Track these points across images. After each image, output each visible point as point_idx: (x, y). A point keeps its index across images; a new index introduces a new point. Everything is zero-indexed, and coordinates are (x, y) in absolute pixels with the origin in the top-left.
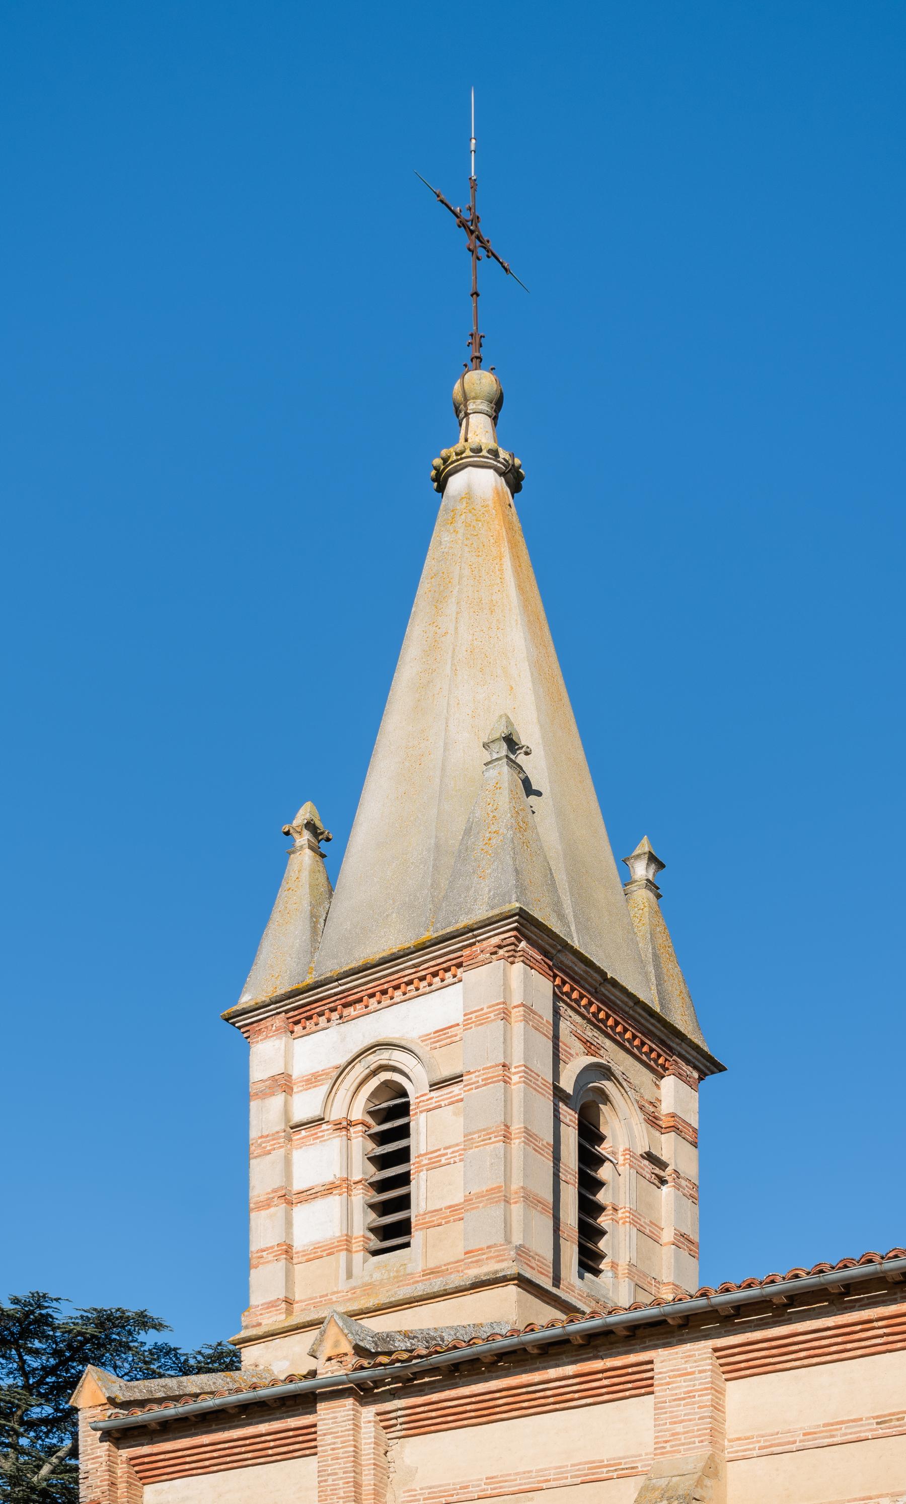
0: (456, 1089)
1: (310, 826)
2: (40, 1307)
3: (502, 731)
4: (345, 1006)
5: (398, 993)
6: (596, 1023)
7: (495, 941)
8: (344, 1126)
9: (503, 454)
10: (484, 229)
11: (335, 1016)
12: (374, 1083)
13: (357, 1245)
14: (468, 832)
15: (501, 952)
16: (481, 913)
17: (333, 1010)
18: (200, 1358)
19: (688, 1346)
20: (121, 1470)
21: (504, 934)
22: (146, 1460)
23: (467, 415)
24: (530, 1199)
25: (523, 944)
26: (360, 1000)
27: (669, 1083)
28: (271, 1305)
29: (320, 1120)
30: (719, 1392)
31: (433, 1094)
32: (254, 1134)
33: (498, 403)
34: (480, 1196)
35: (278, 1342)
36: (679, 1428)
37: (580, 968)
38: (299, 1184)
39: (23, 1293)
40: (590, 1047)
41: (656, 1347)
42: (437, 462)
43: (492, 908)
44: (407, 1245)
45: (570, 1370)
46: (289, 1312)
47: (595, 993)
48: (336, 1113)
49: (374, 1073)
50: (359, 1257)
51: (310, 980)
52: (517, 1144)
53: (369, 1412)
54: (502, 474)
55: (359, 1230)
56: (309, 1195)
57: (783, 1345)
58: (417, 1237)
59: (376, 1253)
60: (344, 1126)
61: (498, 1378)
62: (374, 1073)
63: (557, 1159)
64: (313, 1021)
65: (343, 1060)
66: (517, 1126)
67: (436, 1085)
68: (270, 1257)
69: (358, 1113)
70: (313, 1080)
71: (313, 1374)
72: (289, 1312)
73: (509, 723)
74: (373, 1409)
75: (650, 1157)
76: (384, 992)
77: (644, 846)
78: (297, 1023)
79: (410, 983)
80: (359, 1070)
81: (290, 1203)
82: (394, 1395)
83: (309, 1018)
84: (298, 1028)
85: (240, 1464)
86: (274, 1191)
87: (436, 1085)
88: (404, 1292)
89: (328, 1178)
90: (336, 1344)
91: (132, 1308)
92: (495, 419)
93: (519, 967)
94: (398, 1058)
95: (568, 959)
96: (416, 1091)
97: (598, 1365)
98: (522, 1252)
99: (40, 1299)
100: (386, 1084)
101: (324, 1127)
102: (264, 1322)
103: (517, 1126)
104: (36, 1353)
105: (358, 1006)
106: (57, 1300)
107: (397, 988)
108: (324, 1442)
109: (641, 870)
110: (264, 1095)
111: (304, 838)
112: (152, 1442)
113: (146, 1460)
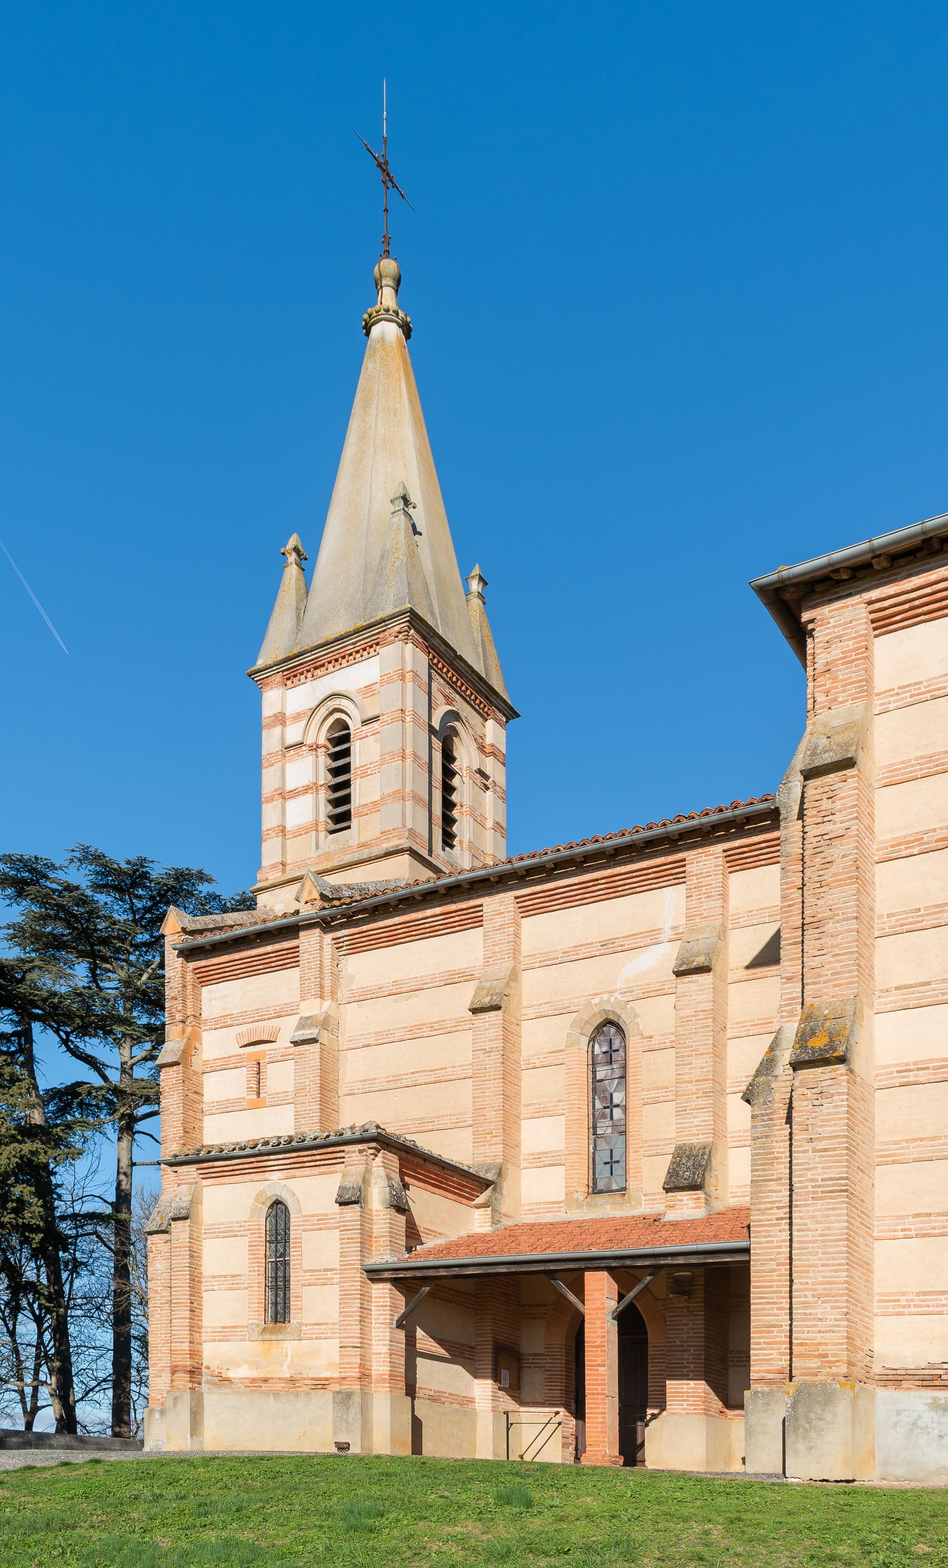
0: (376, 725)
1: (296, 550)
2: (143, 866)
3: (400, 493)
4: (316, 668)
5: (344, 661)
6: (451, 684)
7: (397, 628)
8: (315, 748)
9: (401, 314)
10: (391, 169)
11: (309, 675)
12: (331, 720)
13: (321, 828)
14: (382, 557)
15: (400, 636)
16: (390, 610)
17: (308, 671)
18: (233, 902)
19: (501, 895)
20: (189, 976)
21: (400, 625)
22: (203, 970)
23: (381, 287)
24: (416, 798)
25: (412, 631)
26: (323, 665)
27: (490, 723)
28: (274, 866)
29: (301, 744)
30: (518, 925)
31: (364, 728)
32: (264, 752)
33: (398, 281)
34: (389, 795)
35: (278, 891)
36: (497, 949)
37: (442, 648)
38: (289, 787)
39: (133, 858)
40: (449, 701)
41: (484, 896)
42: (366, 316)
43: (396, 607)
44: (349, 827)
45: (438, 910)
46: (284, 871)
47: (451, 665)
48: (310, 740)
49: (331, 713)
50: (322, 834)
51: (295, 651)
52: (409, 761)
53: (328, 938)
54: (400, 326)
55: (323, 818)
56: (295, 793)
57: (551, 895)
58: (354, 822)
59: (332, 832)
60: (315, 748)
61: (399, 915)
62: (331, 713)
63: (430, 772)
64: (297, 678)
65: (314, 705)
66: (409, 750)
67: (365, 722)
68: (273, 834)
69: (322, 740)
70: (297, 717)
71: (297, 912)
72: (284, 871)
73: (405, 488)
74: (330, 936)
75: (480, 772)
76: (337, 660)
77: (476, 571)
78: (288, 679)
79: (357, 652)
80: (323, 712)
81: (284, 798)
82: (342, 926)
83: (295, 676)
84: (289, 682)
85: (256, 973)
86: (276, 790)
87: (365, 722)
88: (347, 859)
89: (306, 782)
90: (310, 893)
91: (195, 868)
92: (397, 291)
93: (410, 645)
94: (344, 704)
95: (436, 642)
96: (354, 726)
97: (453, 907)
98: (412, 833)
99: (142, 861)
100: (338, 721)
101: (304, 748)
102: (270, 878)
103: (409, 750)
104: (139, 897)
105: (323, 669)
106: (152, 862)
107: (343, 657)
108: (304, 957)
109: (475, 586)
110: (271, 726)
111: (292, 558)
112: (206, 958)
113: (203, 970)
